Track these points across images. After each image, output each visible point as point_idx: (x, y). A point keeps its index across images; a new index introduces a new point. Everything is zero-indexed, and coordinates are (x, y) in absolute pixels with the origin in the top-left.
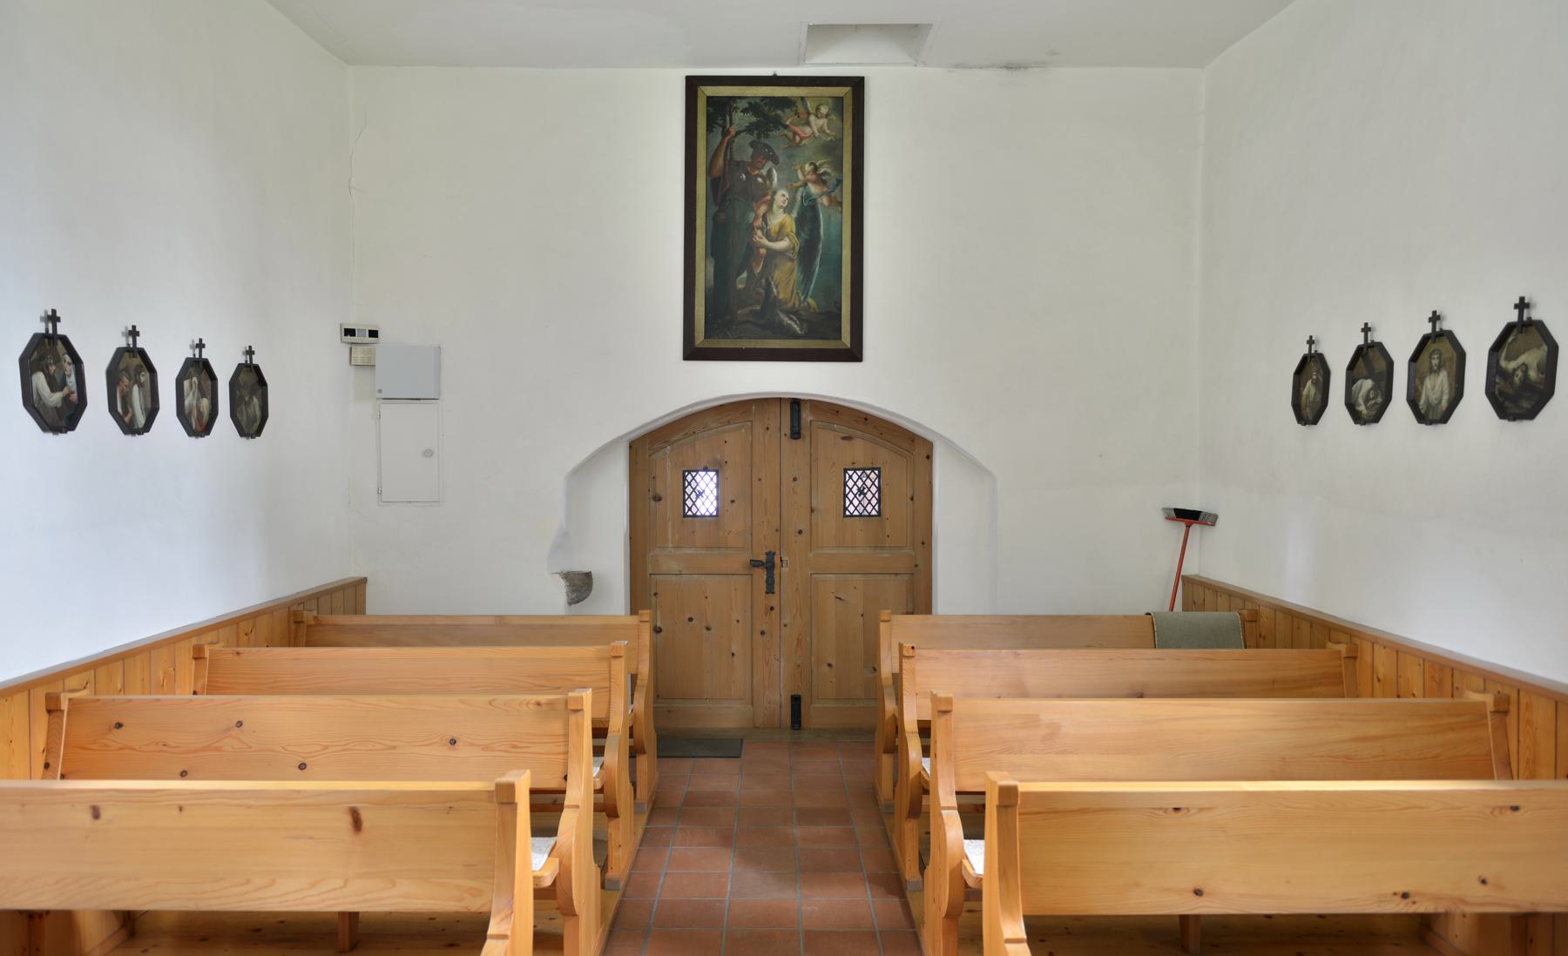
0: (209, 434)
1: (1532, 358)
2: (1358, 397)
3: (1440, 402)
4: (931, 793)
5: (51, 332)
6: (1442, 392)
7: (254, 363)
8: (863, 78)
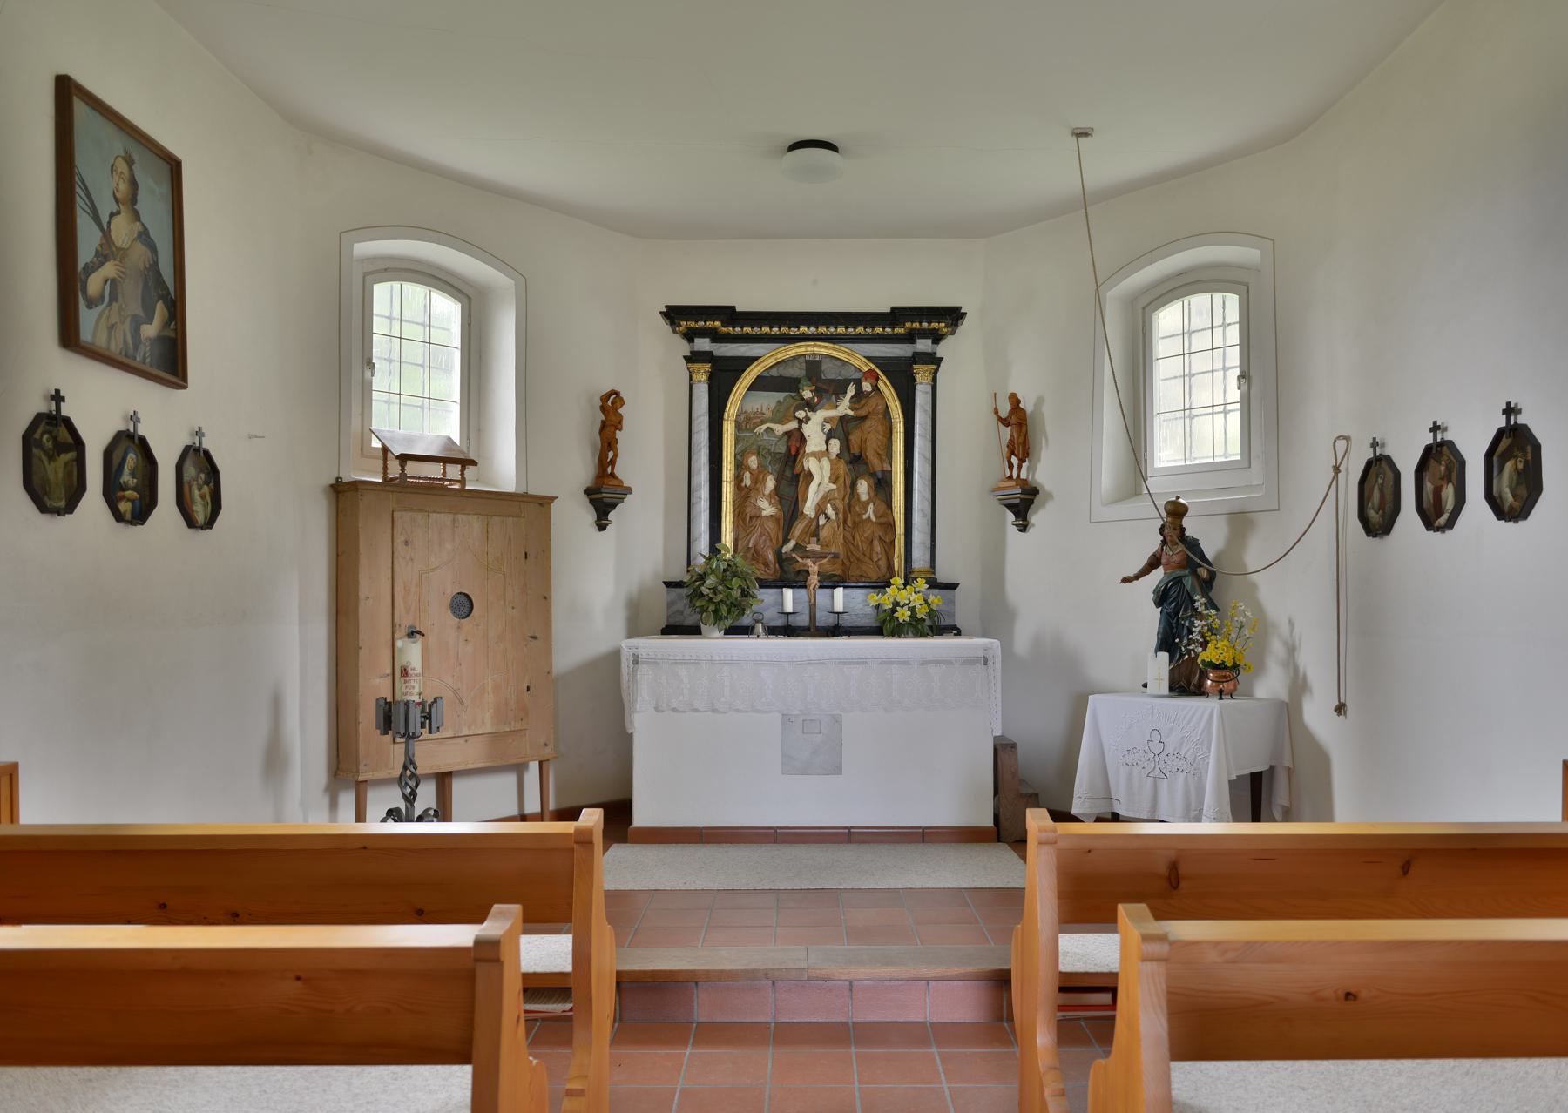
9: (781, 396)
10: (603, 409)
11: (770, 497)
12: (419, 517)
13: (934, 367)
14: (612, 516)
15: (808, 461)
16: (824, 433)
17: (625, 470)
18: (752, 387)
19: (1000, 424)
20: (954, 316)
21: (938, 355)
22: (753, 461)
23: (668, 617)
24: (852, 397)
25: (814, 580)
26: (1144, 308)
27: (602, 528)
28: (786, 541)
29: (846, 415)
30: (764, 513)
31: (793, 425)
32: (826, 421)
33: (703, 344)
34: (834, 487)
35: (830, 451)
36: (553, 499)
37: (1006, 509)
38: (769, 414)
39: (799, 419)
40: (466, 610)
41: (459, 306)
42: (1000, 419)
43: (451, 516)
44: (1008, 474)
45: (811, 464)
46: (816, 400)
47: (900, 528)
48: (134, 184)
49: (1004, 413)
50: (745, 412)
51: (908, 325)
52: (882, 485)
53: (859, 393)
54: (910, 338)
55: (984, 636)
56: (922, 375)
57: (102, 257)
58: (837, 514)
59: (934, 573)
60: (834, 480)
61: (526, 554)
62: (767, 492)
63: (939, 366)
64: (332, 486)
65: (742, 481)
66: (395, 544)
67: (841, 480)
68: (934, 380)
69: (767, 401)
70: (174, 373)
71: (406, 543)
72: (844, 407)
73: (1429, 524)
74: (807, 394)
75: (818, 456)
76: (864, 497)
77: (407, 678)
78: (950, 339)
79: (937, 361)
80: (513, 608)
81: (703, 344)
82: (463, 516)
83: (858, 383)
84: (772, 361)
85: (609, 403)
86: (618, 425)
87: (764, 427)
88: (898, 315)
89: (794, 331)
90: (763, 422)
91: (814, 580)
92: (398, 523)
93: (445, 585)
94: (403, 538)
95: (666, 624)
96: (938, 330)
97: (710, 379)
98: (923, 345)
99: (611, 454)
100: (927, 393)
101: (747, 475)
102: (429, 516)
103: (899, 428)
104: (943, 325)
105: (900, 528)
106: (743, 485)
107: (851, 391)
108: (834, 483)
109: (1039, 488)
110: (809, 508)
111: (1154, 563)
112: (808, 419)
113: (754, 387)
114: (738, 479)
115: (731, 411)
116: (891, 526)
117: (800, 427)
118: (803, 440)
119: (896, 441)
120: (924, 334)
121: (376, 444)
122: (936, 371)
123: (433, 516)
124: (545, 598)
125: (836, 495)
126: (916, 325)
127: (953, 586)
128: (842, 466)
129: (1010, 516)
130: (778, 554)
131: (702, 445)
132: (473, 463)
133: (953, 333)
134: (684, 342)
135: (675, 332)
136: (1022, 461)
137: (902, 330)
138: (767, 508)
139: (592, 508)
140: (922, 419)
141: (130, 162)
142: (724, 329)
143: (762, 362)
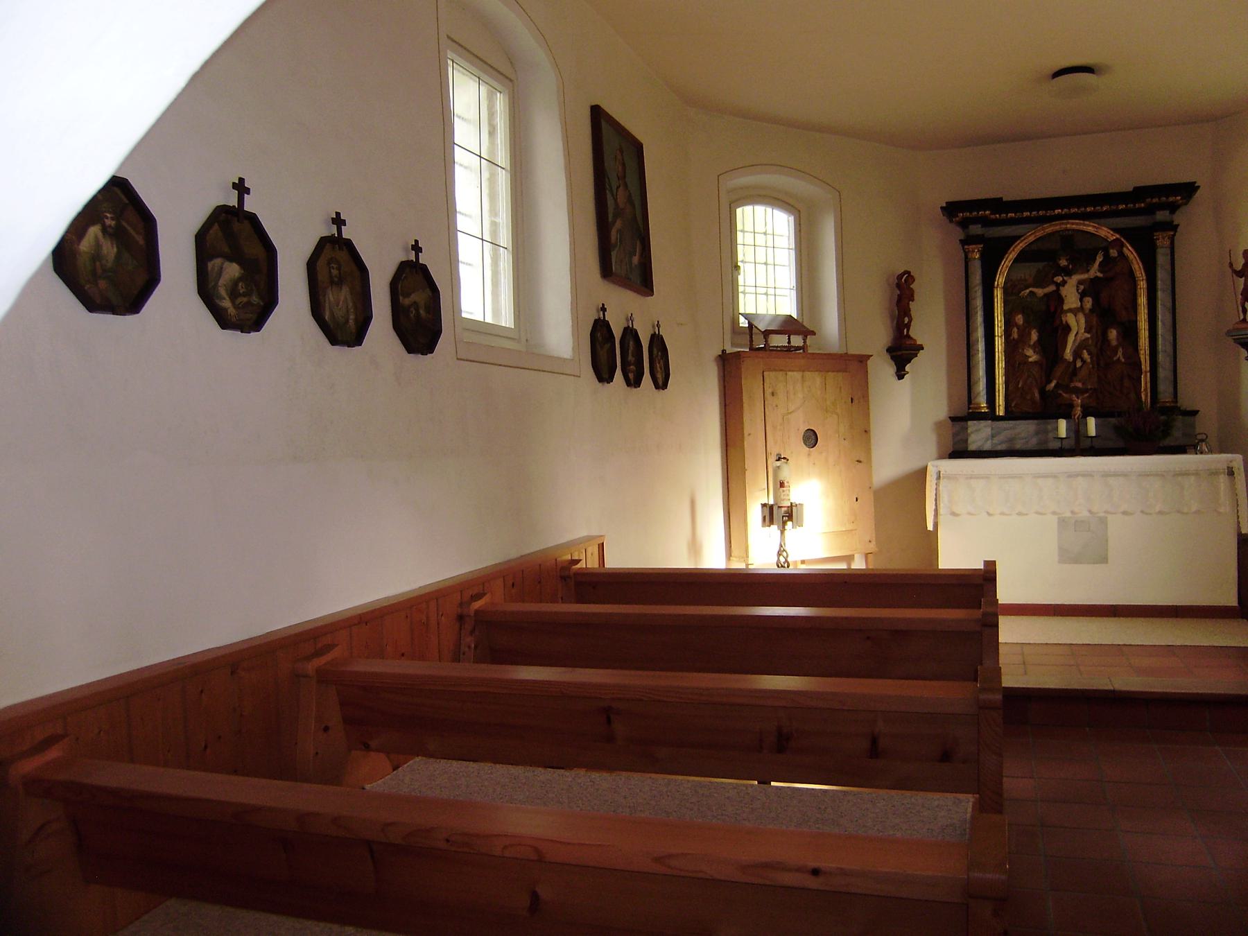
0: (258, 330)
1: (420, 297)
2: (216, 285)
3: (347, 321)
4: (901, 381)
5: (657, 333)
6: (348, 311)
7: (421, 262)
8: (995, 562)
9: (1040, 265)
10: (899, 286)
11: (1034, 347)
12: (780, 375)
13: (1172, 233)
14: (907, 368)
15: (1066, 316)
16: (1079, 293)
17: (918, 332)
18: (1016, 260)
19: (1234, 276)
20: (1189, 190)
21: (1175, 223)
22: (1019, 319)
23: (954, 444)
24: (1100, 263)
25: (1078, 411)
27: (900, 376)
29: (1097, 277)
30: (1030, 360)
31: (1052, 288)
32: (1080, 282)
33: (976, 229)
34: (1089, 336)
35: (1084, 307)
36: (869, 357)
37: (1240, 347)
40: (813, 442)
41: (792, 219)
43: (801, 373)
44: (1242, 317)
45: (1071, 319)
46: (1071, 266)
47: (1146, 366)
48: (624, 165)
49: (1239, 266)
50: (1011, 280)
52: (1130, 333)
53: (1107, 263)
54: (1150, 210)
55: (1221, 451)
56: (1162, 241)
57: (616, 216)
59: (1177, 402)
60: (1088, 330)
61: (852, 399)
62: (1032, 343)
63: (1176, 231)
64: (720, 356)
65: (1010, 335)
66: (765, 395)
67: (1094, 331)
68: (1172, 243)
69: (1028, 271)
70: (646, 286)
71: (773, 394)
72: (1094, 271)
74: (1063, 263)
75: (1074, 312)
76: (1114, 343)
77: (784, 489)
78: (1184, 209)
79: (1175, 228)
80: (845, 439)
81: (976, 229)
82: (809, 373)
83: (1106, 251)
84: (1032, 239)
85: (903, 280)
86: (911, 298)
87: (1028, 291)
88: (1141, 192)
89: (1049, 213)
90: (1027, 288)
91: (1078, 411)
92: (767, 380)
93: (800, 424)
94: (770, 390)
95: (952, 450)
96: (1175, 202)
97: (982, 257)
98: (1161, 216)
99: (906, 320)
100: (1167, 255)
101: (1015, 330)
102: (786, 374)
103: (1142, 285)
104: (1179, 198)
105: (1146, 366)
106: (1012, 338)
107: (1099, 259)
108: (1088, 333)
110: (1068, 354)
112: (1064, 283)
114: (1007, 333)
115: (1000, 280)
116: (1137, 365)
117: (1058, 290)
118: (1061, 300)
119: (1141, 296)
120: (1162, 207)
121: (743, 323)
122: (1174, 235)
123: (789, 373)
124: (866, 431)
125: (1090, 342)
126: (1155, 200)
128: (1095, 319)
130: (1043, 392)
131: (978, 308)
132: (813, 333)
133: (1186, 204)
134: (959, 229)
135: (951, 221)
137: (1143, 205)
138: (1032, 355)
139: (893, 363)
140: (1162, 275)
141: (622, 152)
142: (993, 216)
143: (1024, 239)
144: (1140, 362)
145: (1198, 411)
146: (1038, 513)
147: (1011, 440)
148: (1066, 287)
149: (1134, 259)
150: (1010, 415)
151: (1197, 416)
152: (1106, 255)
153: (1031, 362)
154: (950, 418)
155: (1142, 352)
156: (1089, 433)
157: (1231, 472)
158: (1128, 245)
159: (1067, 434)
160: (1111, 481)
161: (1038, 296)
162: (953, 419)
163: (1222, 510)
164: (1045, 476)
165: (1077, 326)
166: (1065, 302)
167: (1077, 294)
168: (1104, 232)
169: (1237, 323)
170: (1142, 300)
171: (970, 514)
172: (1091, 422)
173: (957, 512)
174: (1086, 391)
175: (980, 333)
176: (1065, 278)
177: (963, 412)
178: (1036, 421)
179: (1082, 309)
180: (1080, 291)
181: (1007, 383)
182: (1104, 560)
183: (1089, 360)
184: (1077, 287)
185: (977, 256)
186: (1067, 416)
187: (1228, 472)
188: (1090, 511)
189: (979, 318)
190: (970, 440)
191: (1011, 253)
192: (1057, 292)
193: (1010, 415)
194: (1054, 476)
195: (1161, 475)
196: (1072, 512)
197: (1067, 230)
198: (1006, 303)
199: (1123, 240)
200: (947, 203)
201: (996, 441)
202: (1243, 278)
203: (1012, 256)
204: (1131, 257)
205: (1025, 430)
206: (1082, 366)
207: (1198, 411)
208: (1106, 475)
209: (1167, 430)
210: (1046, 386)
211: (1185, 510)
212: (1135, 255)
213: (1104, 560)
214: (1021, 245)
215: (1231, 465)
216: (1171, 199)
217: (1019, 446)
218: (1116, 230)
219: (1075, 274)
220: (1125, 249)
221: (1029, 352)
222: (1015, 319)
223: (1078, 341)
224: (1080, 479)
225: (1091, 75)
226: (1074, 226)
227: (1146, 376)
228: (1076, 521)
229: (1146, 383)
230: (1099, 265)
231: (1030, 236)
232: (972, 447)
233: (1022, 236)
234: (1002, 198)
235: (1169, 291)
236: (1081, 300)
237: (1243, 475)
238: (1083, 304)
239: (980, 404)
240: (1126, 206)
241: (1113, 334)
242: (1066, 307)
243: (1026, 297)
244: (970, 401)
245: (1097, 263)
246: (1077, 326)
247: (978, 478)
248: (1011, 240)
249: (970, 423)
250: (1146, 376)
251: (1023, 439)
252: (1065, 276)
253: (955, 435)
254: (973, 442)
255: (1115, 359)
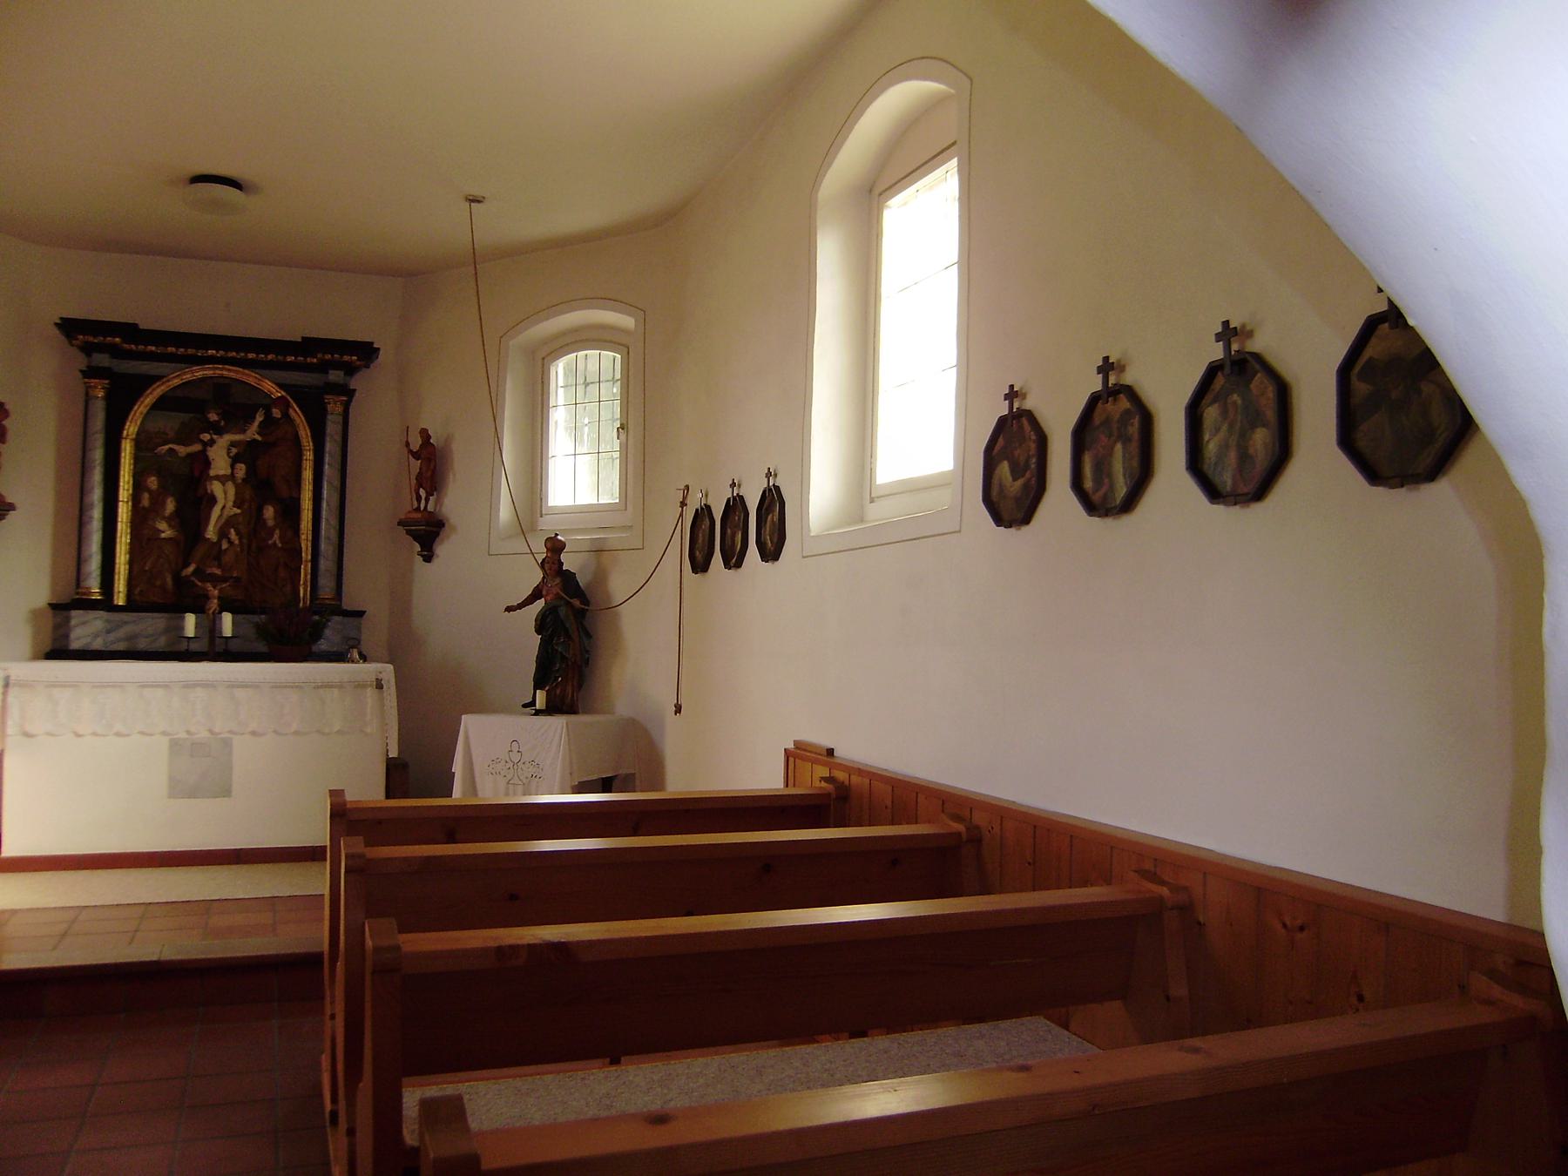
8: (343, 790)
9: (185, 417)
11: (169, 520)
16: (230, 457)
19: (410, 456)
22: (153, 482)
24: (261, 422)
26: (543, 359)
28: (186, 565)
29: (254, 440)
30: (163, 535)
31: (197, 447)
32: (233, 444)
33: (102, 360)
34: (239, 511)
38: (171, 434)
39: (204, 441)
42: (411, 452)
45: (217, 488)
46: (222, 423)
47: (306, 554)
51: (319, 355)
52: (290, 512)
53: (269, 422)
54: (323, 367)
56: (334, 407)
58: (240, 539)
60: (236, 505)
65: (139, 502)
69: (170, 422)
72: (252, 433)
73: (727, 565)
74: (213, 417)
75: (222, 479)
79: (350, 393)
81: (102, 360)
84: (176, 382)
87: (167, 447)
88: (309, 345)
97: (109, 398)
98: (335, 376)
101: (146, 496)
103: (309, 456)
105: (306, 554)
106: (141, 505)
107: (259, 418)
108: (238, 508)
109: (445, 521)
110: (211, 533)
111: (536, 595)
112: (212, 442)
113: (159, 405)
114: (136, 498)
115: (131, 429)
118: (207, 464)
119: (306, 469)
125: (241, 519)
126: (328, 357)
127: (360, 614)
129: (418, 548)
130: (177, 579)
136: (429, 494)
137: (315, 360)
140: (330, 446)
144: (301, 548)
145: (365, 612)
146: (142, 733)
147: (131, 638)
148: (215, 447)
149: (301, 424)
150: (132, 606)
151: (365, 617)
152: (268, 415)
153: (164, 539)
154: (49, 604)
155: (303, 537)
156: (186, 631)
157: (379, 685)
158: (295, 407)
159: (196, 632)
160: (240, 694)
161: (180, 455)
162: (54, 607)
163: (369, 730)
164: (244, 686)
165: (224, 497)
166: (212, 466)
167: (227, 458)
168: (268, 386)
169: (409, 512)
170: (308, 475)
171: (50, 734)
172: (227, 619)
173: (81, 733)
174: (225, 580)
175: (96, 495)
176: (215, 437)
177: (64, 599)
178: (166, 615)
179: (232, 477)
180: (231, 454)
181: (131, 563)
182: (226, 792)
183: (237, 542)
184: (229, 449)
185: (101, 394)
186: (198, 610)
187: (377, 684)
188: (211, 731)
189: (97, 476)
190: (73, 636)
191: (148, 396)
192: (203, 454)
193: (132, 606)
194: (166, 686)
195: (278, 686)
196: (188, 732)
197: (222, 377)
198: (137, 459)
199: (289, 398)
200: (303, 338)
201: (112, 637)
202: (419, 461)
203: (149, 399)
204: (298, 421)
205: (150, 625)
206: (227, 549)
207: (365, 612)
208: (233, 685)
209: (317, 634)
210: (182, 571)
211: (327, 731)
212: (303, 419)
213: (226, 792)
214: (162, 388)
215: (380, 676)
216: (346, 358)
217: (142, 645)
218: (281, 386)
219: (227, 433)
220: (291, 410)
221: (162, 526)
222: (146, 481)
223: (225, 517)
224: (199, 690)
225: (238, 191)
226: (232, 374)
227: (306, 566)
228: (192, 744)
229: (306, 576)
230: (259, 426)
231: (178, 378)
232: (75, 645)
233: (163, 377)
234: (372, 343)
235: (338, 466)
236: (232, 467)
237: (393, 689)
238: (235, 471)
239: (90, 588)
240: (296, 359)
241: (269, 512)
242: (212, 473)
243: (165, 453)
244: (78, 584)
245: (256, 424)
246: (224, 497)
247: (65, 686)
248: (149, 381)
249: (74, 613)
250: (306, 566)
251: (147, 637)
252: (215, 434)
253: (56, 627)
254: (78, 639)
255: (270, 542)
